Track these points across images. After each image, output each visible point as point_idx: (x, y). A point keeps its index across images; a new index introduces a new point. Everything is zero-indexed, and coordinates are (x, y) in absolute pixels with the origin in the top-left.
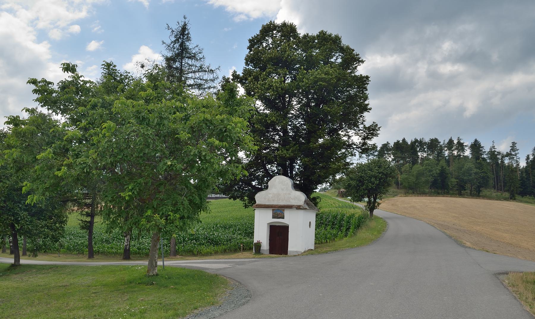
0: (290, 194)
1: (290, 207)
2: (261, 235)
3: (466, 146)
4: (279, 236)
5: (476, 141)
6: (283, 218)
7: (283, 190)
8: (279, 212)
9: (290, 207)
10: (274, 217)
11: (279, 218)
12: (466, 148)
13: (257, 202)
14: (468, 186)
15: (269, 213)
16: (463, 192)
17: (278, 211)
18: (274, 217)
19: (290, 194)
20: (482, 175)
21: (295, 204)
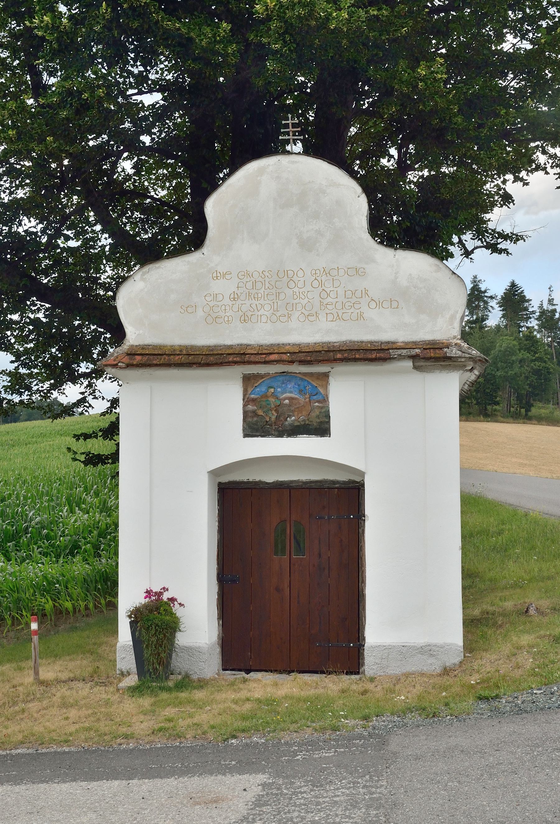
0: (358, 272)
1: (375, 355)
2: (167, 553)
3: (491, 297)
4: (291, 561)
5: (513, 285)
6: (321, 429)
7: (307, 245)
8: (288, 393)
9: (375, 355)
10: (254, 427)
11: (295, 431)
12: (493, 303)
13: (135, 335)
14: (501, 395)
15: (224, 399)
16: (489, 407)
17: (286, 385)
18: (254, 427)
19: (358, 272)
20: (537, 365)
21: (401, 336)
